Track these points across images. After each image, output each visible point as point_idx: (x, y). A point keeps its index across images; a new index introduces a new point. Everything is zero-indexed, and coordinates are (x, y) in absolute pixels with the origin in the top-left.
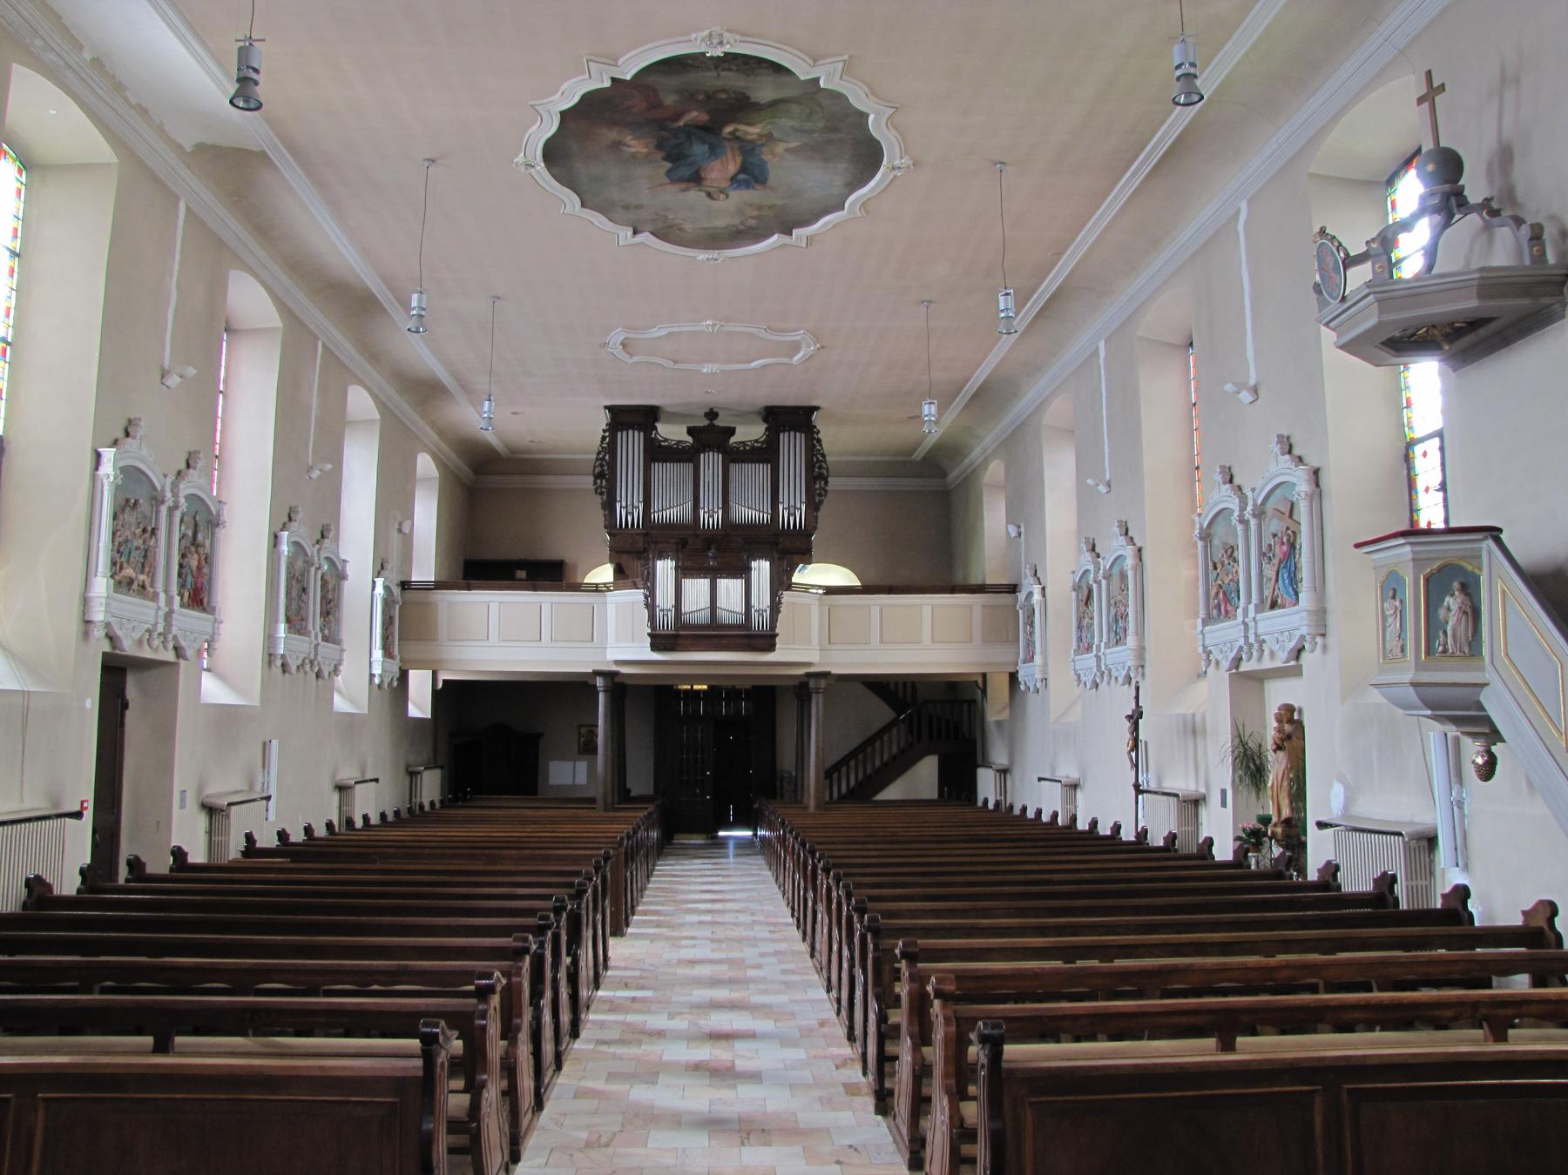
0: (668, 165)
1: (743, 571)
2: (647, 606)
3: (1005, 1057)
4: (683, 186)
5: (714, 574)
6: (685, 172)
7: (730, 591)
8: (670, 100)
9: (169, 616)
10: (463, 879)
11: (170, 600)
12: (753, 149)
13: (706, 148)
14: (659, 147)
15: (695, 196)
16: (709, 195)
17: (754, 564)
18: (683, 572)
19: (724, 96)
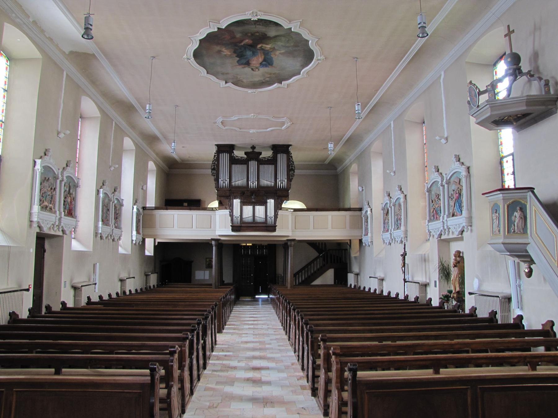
0: (238, 59)
1: (264, 203)
2: (230, 215)
3: (358, 376)
4: (243, 66)
5: (254, 204)
6: (244, 61)
7: (260, 210)
8: (238, 35)
9: (60, 219)
10: (165, 313)
11: (60, 213)
12: (268, 53)
13: (251, 52)
14: (235, 52)
15: (247, 70)
16: (252, 69)
17: (268, 201)
18: (243, 203)
19: (258, 34)
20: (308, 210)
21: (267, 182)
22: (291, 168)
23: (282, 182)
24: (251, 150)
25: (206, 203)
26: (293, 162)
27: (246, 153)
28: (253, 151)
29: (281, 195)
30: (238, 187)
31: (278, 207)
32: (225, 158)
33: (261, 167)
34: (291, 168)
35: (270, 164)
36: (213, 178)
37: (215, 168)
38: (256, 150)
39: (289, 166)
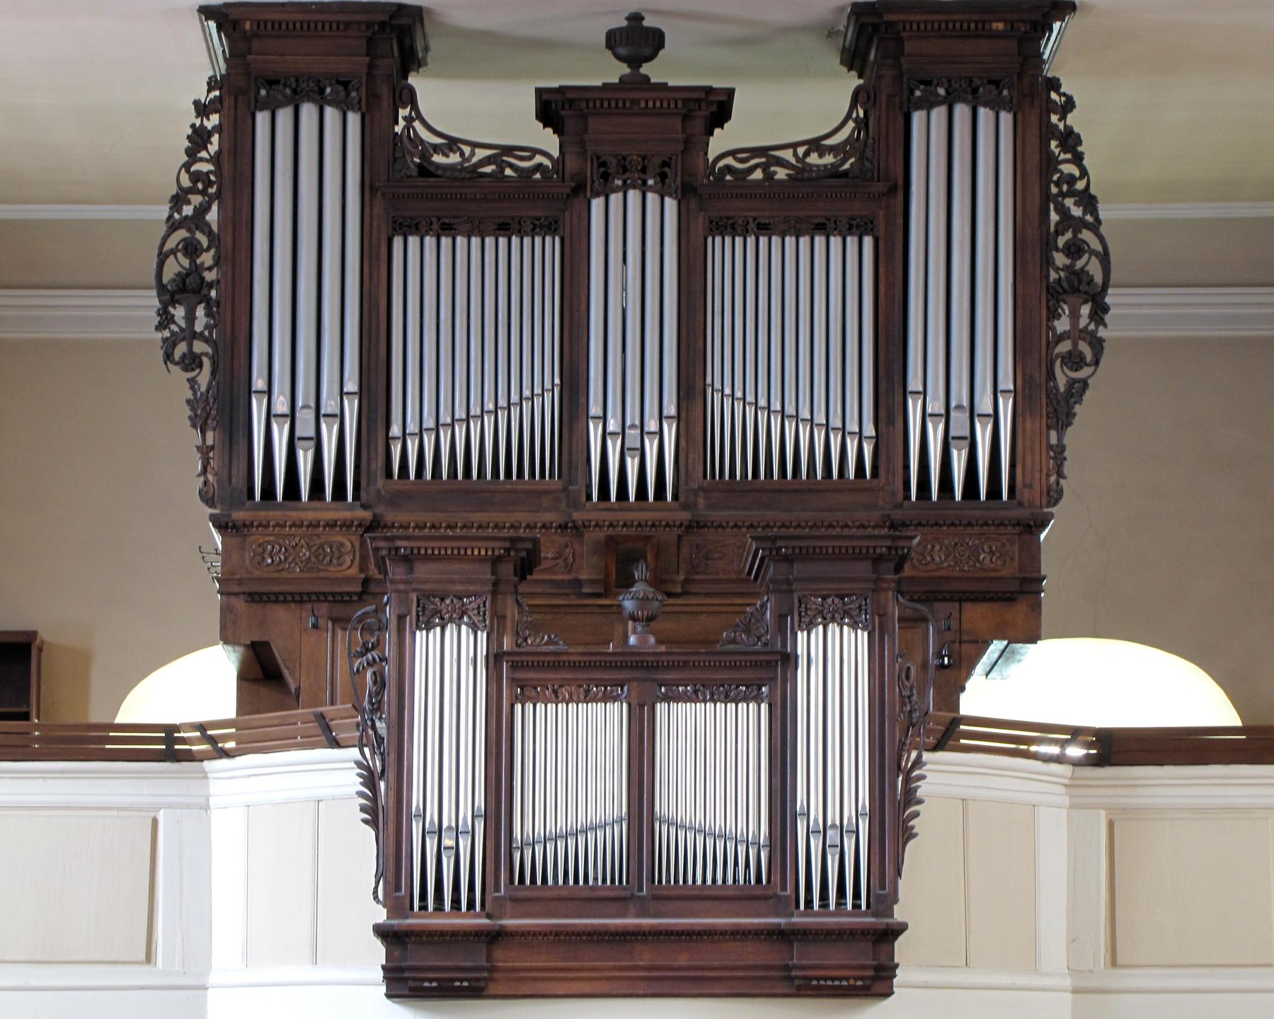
1: (760, 672)
2: (373, 814)
5: (643, 682)
7: (709, 756)
18: (521, 676)
20: (1259, 744)
21: (796, 399)
22: (1059, 269)
23: (963, 407)
24: (611, 71)
25: (99, 681)
26: (1088, 201)
27: (551, 108)
28: (636, 83)
29: (946, 571)
30: (461, 488)
31: (915, 717)
32: (313, 160)
33: (728, 256)
34: (1059, 269)
35: (823, 228)
36: (176, 388)
37: (207, 284)
38: (669, 71)
39: (1048, 245)
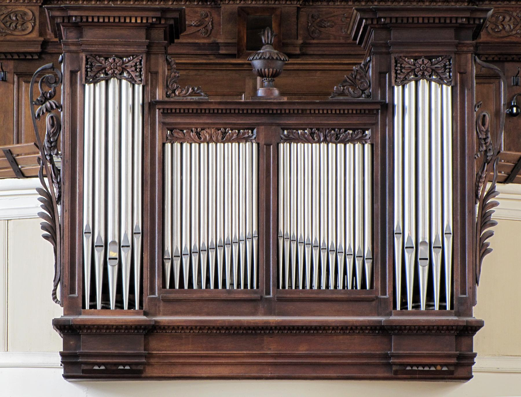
1: (366, 118)
2: (52, 232)
3: (161, 100)
5: (273, 124)
7: (323, 186)
10: (181, 361)
17: (403, 95)
18: (169, 119)
